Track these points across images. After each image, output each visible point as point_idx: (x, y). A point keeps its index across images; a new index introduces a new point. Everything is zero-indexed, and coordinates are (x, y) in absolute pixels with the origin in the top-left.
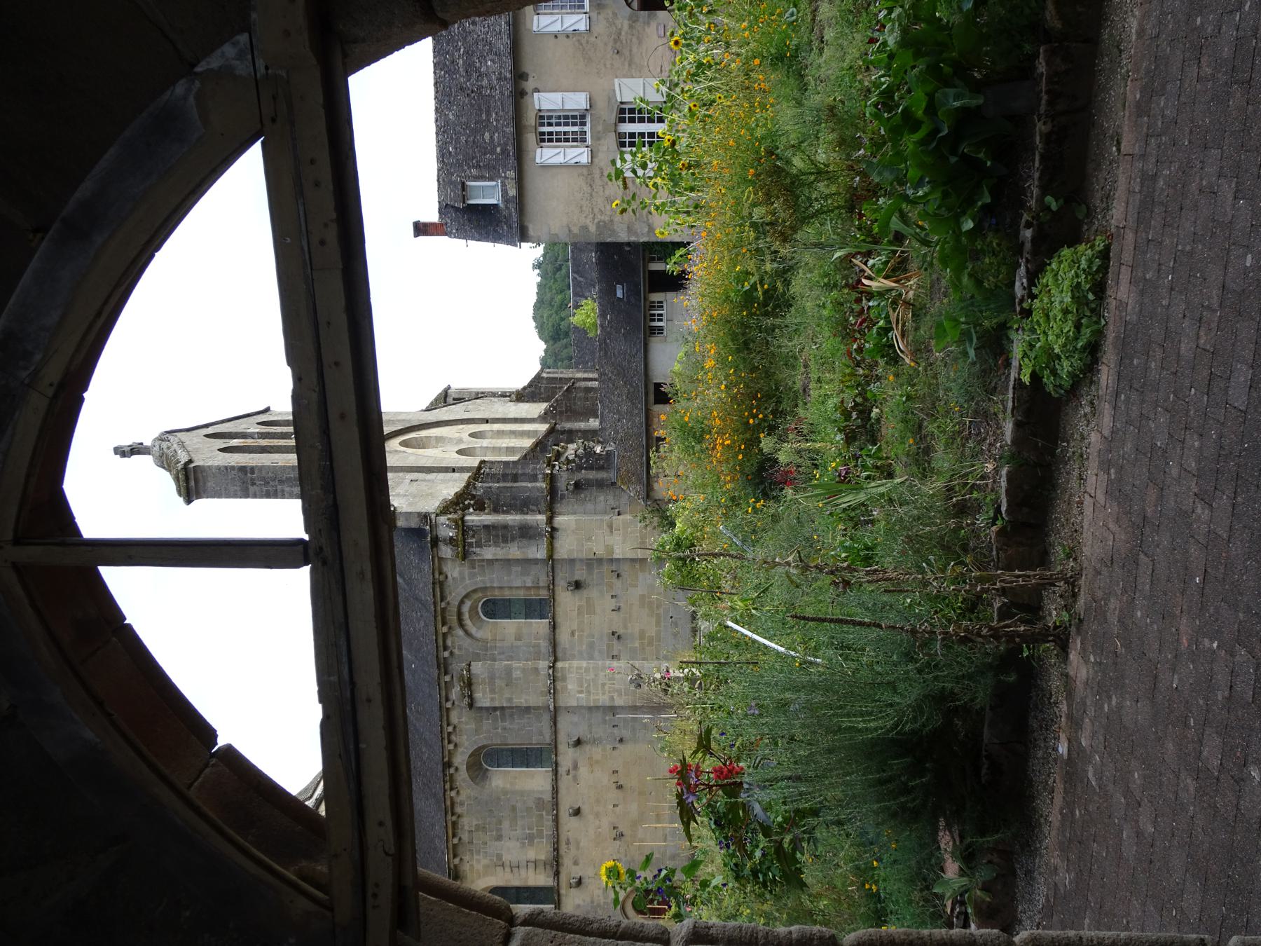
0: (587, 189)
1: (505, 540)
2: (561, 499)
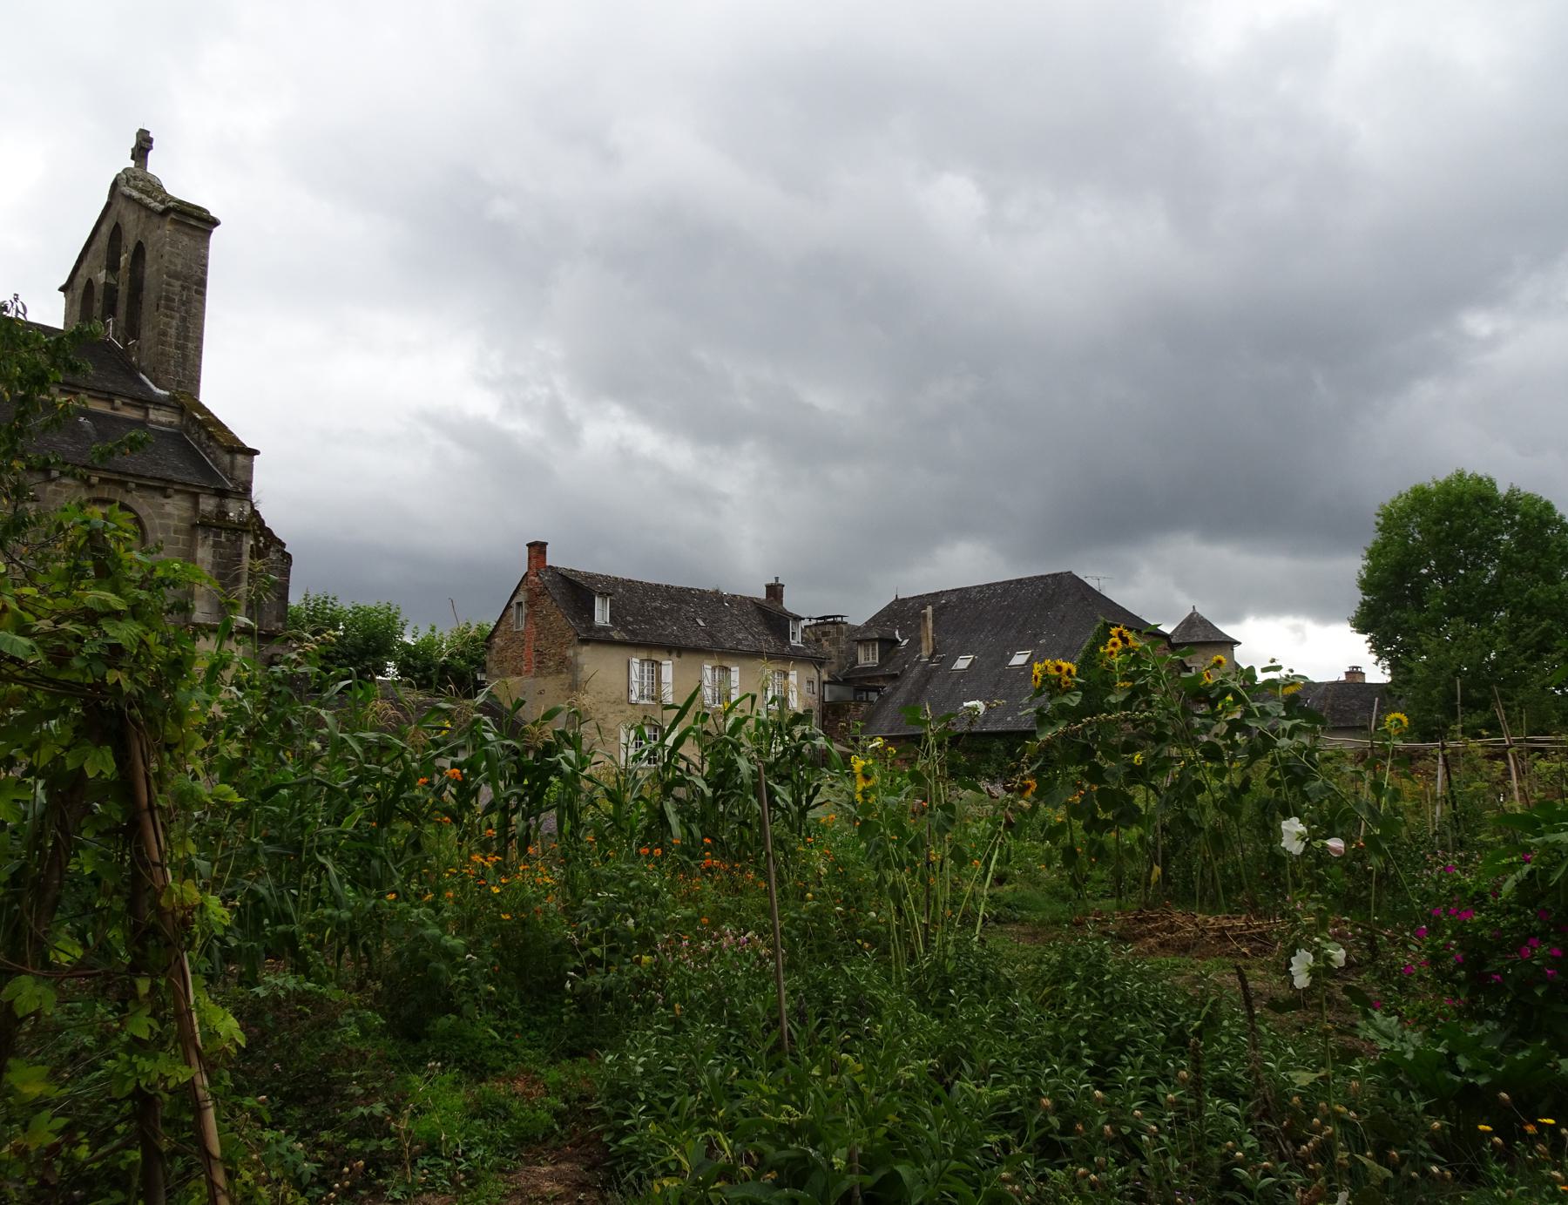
0: (613, 698)
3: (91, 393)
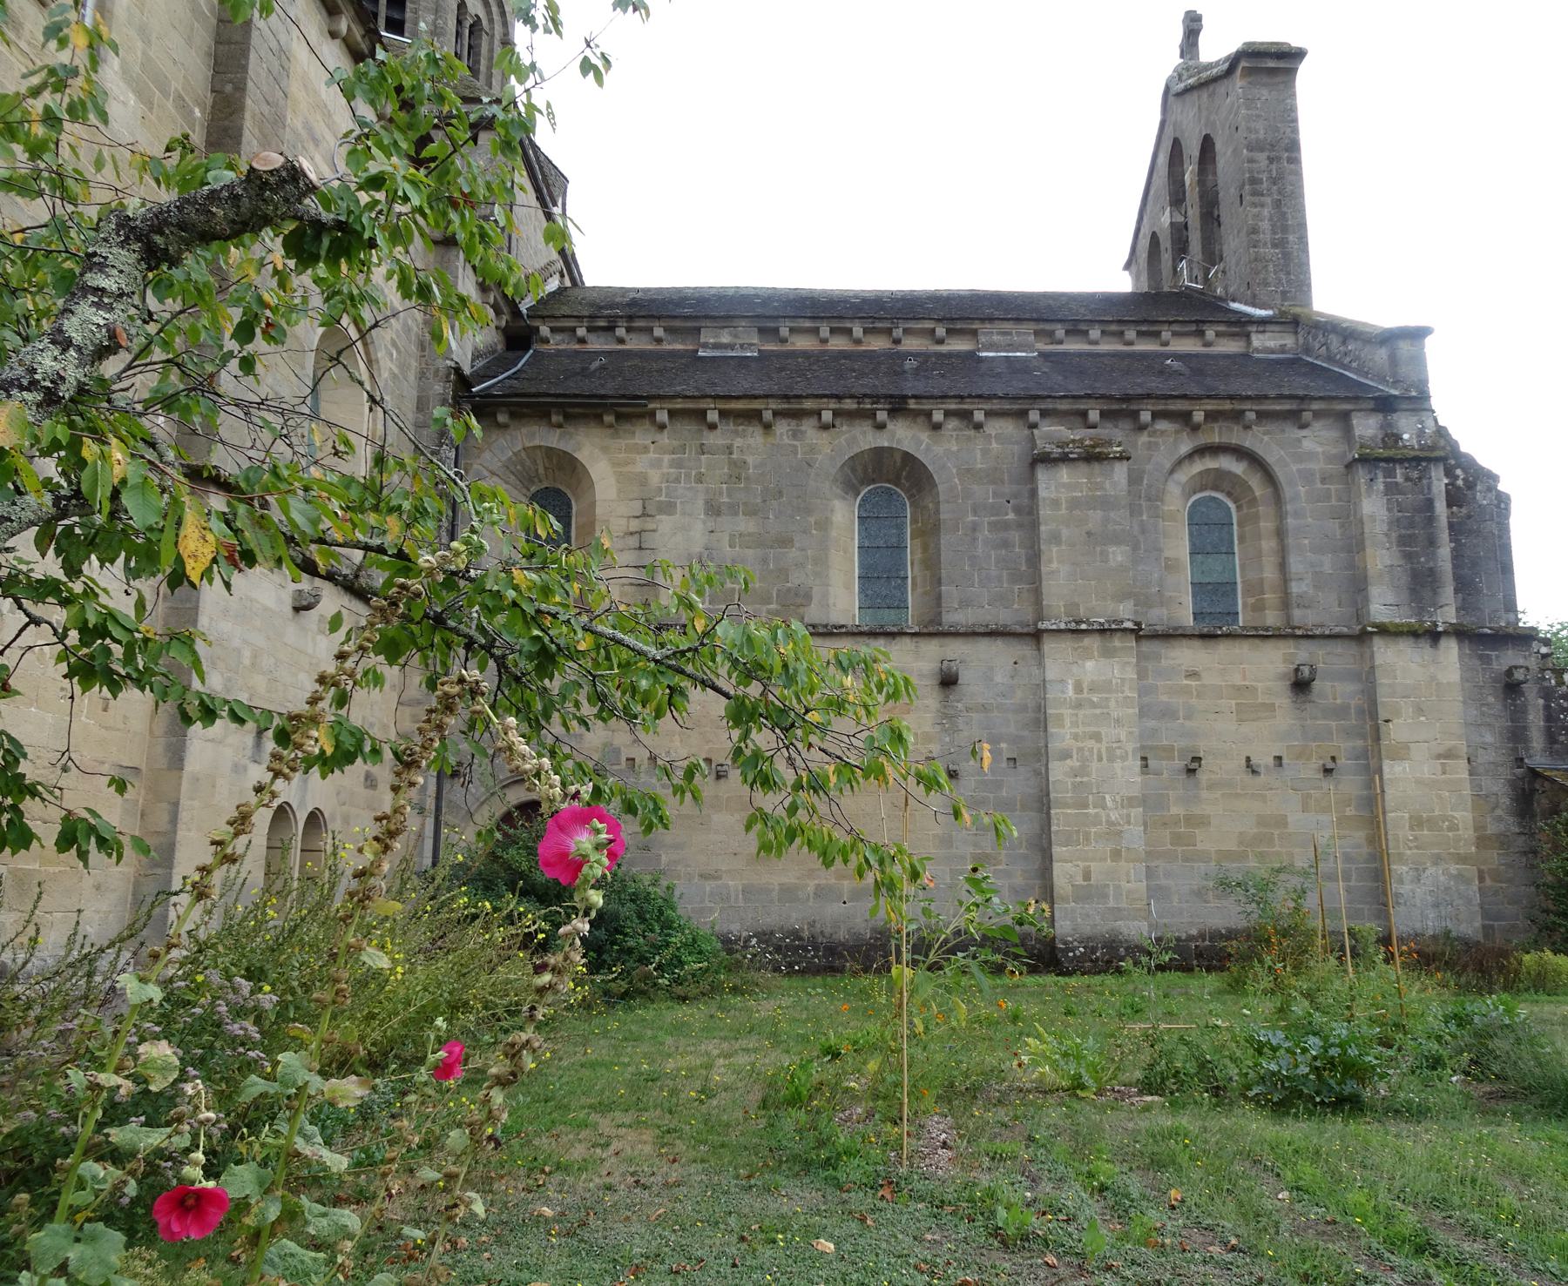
1: (1403, 541)
2: (1481, 657)
3: (1176, 328)
